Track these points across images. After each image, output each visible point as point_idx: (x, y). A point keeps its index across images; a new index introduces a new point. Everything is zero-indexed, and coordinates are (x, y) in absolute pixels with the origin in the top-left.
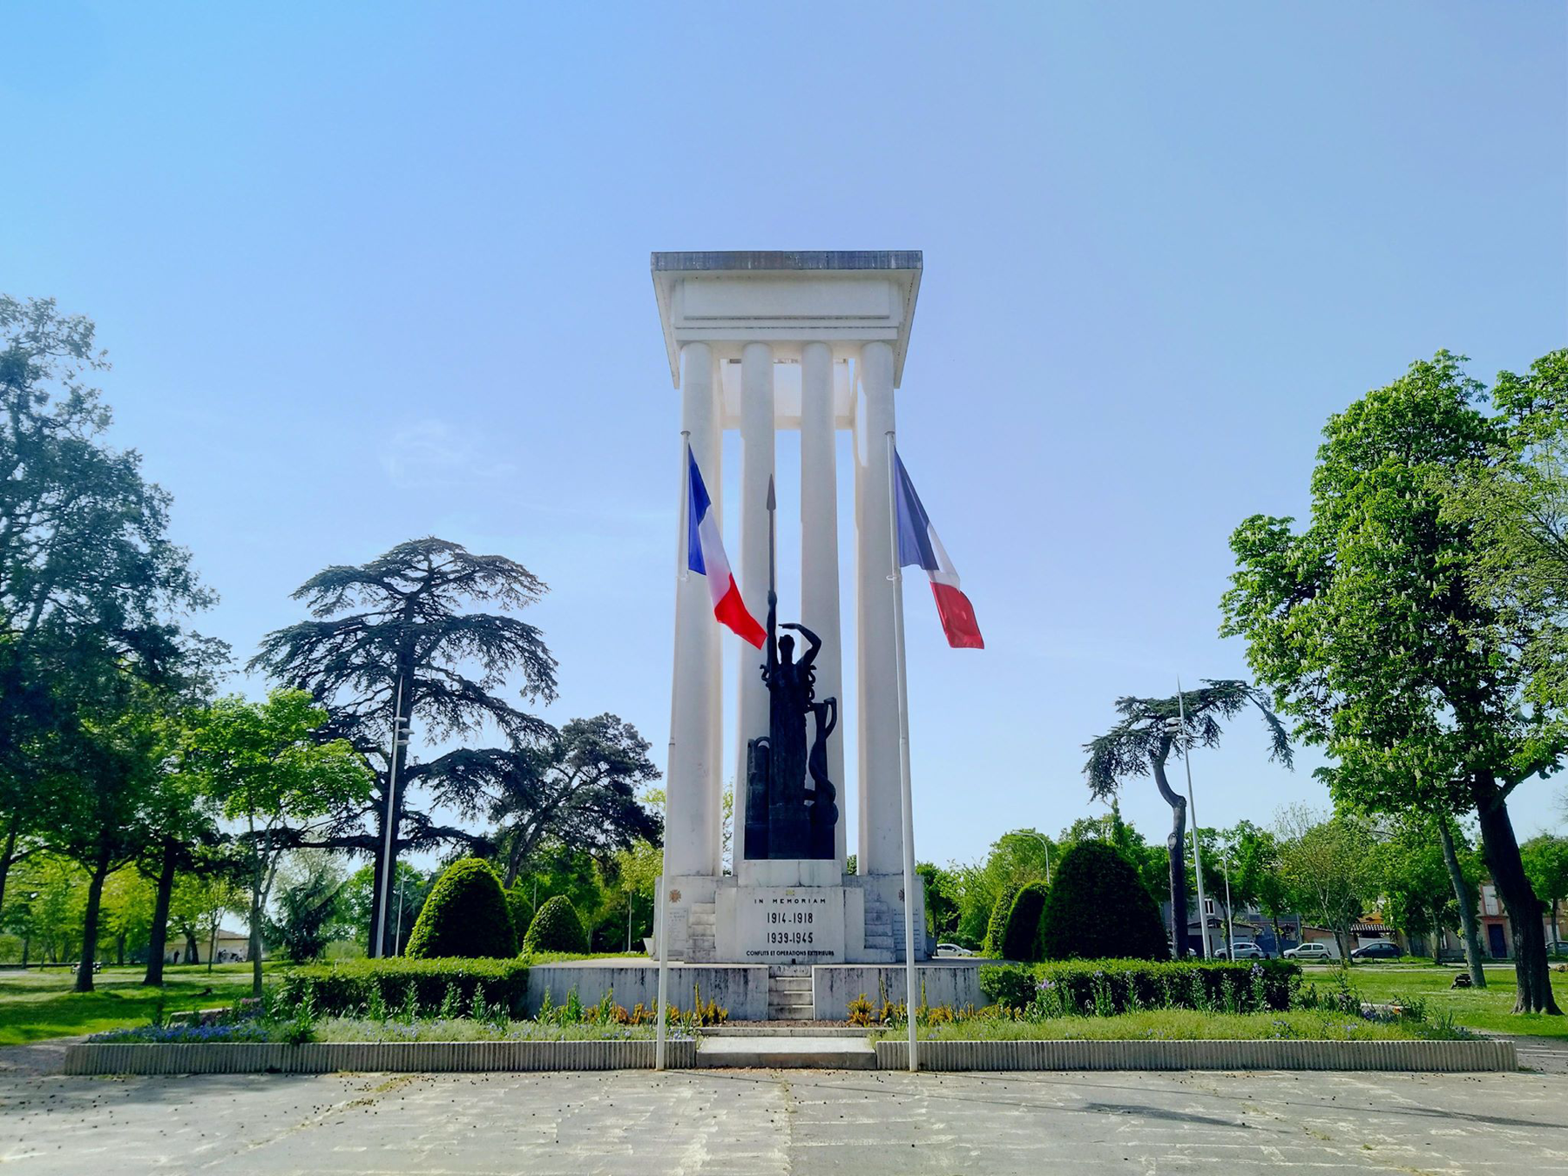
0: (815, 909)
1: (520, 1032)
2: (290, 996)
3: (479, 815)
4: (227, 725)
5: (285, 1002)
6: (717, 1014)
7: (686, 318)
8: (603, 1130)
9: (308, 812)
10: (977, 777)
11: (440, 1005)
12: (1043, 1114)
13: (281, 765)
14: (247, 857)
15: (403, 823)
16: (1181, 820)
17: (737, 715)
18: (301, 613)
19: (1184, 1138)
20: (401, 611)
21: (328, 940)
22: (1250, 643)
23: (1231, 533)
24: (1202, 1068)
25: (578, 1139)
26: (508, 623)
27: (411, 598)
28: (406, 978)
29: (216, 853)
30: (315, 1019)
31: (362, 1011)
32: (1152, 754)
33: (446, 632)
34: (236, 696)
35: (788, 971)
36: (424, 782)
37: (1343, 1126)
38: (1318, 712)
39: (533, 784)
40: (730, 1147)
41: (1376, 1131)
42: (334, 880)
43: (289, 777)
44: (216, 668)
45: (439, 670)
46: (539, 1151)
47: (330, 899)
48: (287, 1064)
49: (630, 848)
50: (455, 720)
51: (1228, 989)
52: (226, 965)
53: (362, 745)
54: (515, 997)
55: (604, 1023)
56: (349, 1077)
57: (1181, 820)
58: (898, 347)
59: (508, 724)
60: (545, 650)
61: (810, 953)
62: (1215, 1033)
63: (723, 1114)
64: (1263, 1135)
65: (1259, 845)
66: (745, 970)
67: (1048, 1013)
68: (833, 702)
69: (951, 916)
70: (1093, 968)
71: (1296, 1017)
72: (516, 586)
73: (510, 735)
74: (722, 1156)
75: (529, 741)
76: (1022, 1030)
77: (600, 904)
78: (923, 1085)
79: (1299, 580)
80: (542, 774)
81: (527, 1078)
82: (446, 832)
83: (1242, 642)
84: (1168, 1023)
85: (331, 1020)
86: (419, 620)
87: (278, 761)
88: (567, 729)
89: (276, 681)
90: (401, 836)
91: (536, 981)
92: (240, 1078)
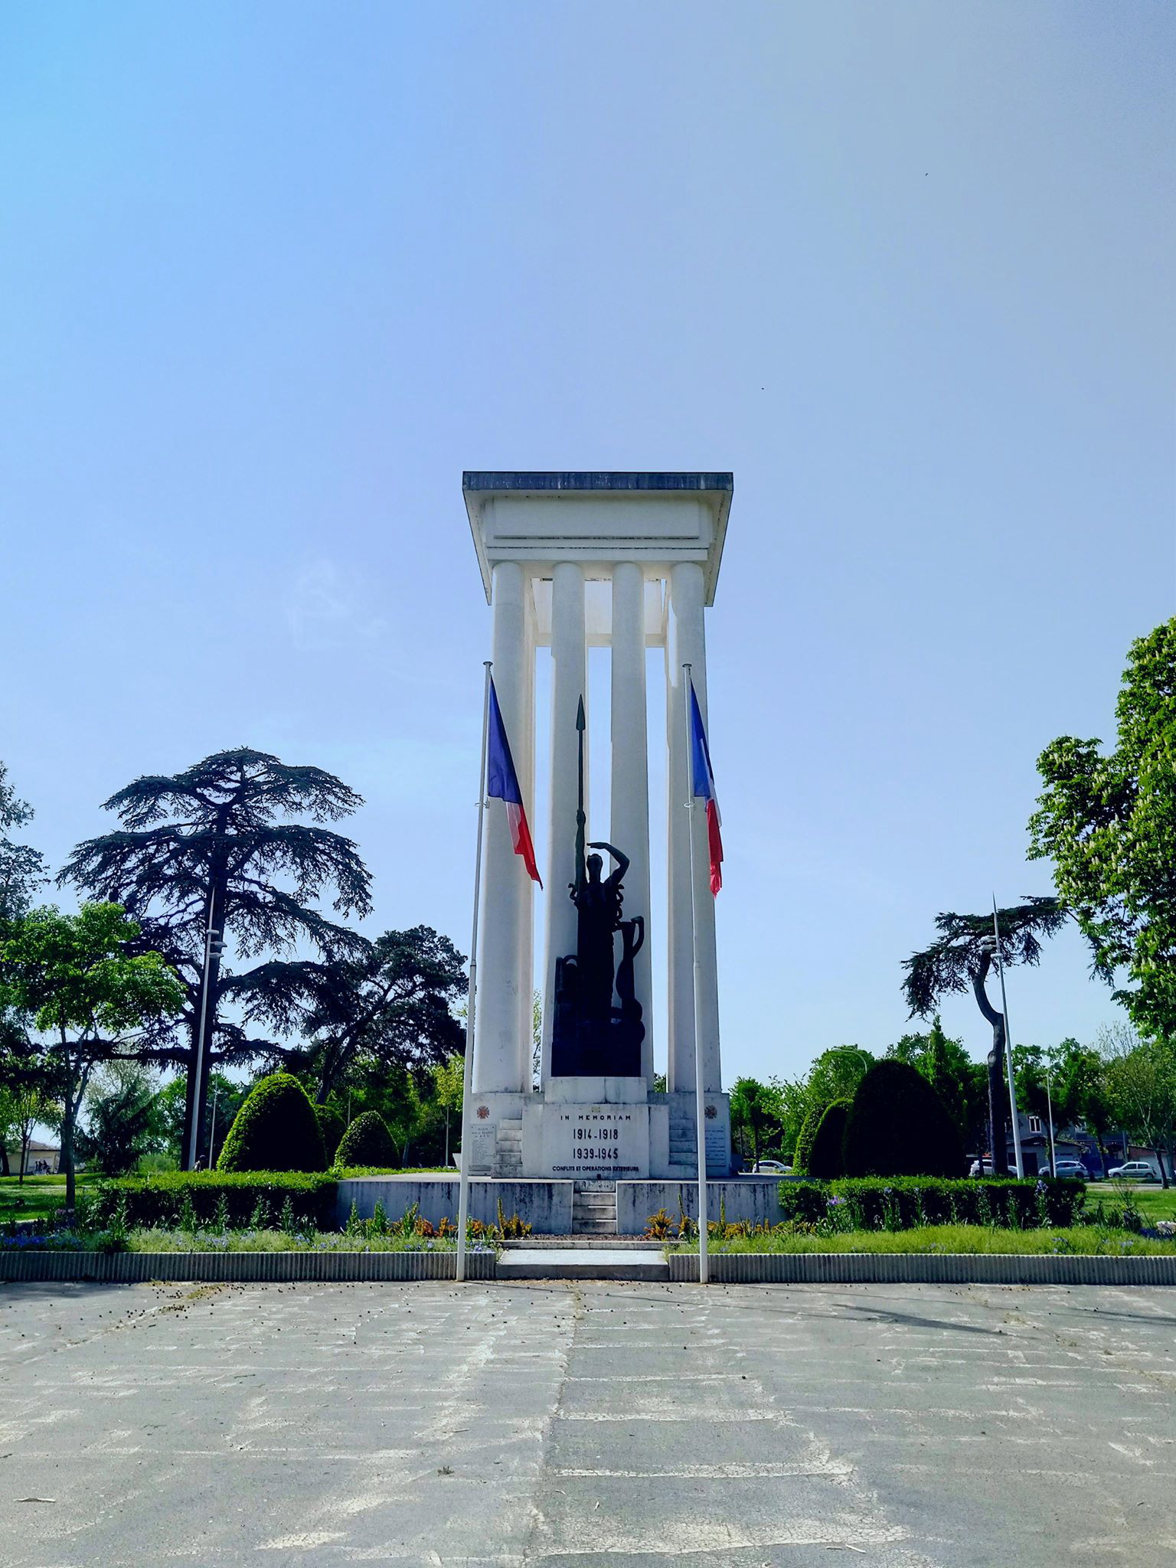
0: (621, 1126)
1: (327, 1243)
2: (104, 1206)
3: (293, 1028)
4: (39, 938)
5: (99, 1212)
6: (519, 1228)
7: (497, 538)
8: (398, 1333)
9: (119, 1024)
10: (789, 996)
11: (249, 1217)
12: (814, 1321)
13: (93, 978)
14: (59, 1067)
15: (216, 1036)
16: (1001, 1039)
17: (543, 931)
18: (112, 823)
19: (940, 1343)
20: (214, 822)
21: (142, 1152)
22: (1056, 864)
23: (1037, 755)
24: (982, 1282)
25: (373, 1341)
26: (322, 835)
27: (225, 809)
28: (216, 1191)
29: (27, 1064)
30: (129, 1229)
31: (175, 1222)
32: (971, 971)
33: (259, 845)
34: (49, 908)
35: (594, 1186)
36: (237, 995)
37: (1094, 1334)
38: (1124, 934)
39: (346, 998)
40: (515, 1348)
41: (1123, 1339)
42: (146, 1092)
43: (101, 990)
44: (27, 877)
45: (251, 881)
46: (337, 1350)
47: (143, 1111)
48: (101, 1273)
49: (445, 1063)
50: (269, 934)
51: (1016, 1208)
52: (37, 1177)
53: (173, 958)
54: (326, 1209)
55: (408, 1235)
56: (161, 1285)
57: (1001, 1039)
58: (710, 568)
59: (322, 938)
60: (359, 863)
61: (615, 1169)
62: (995, 1247)
63: (513, 1321)
64: (1015, 1341)
65: (1084, 1062)
66: (550, 1185)
67: (838, 1226)
68: (640, 921)
69: (772, 1132)
70: (884, 1184)
71: (1081, 1234)
72: (331, 798)
73: (324, 948)
74: (505, 1355)
75: (342, 953)
76: (812, 1244)
77: (416, 1119)
78: (709, 1296)
79: (1103, 802)
80: (357, 986)
81: (332, 1287)
82: (260, 1045)
83: (1049, 865)
84: (952, 1238)
85: (143, 1231)
86: (231, 831)
87: (90, 974)
88: (382, 941)
89: (87, 891)
90: (213, 1050)
91: (345, 1193)
92: (56, 1285)
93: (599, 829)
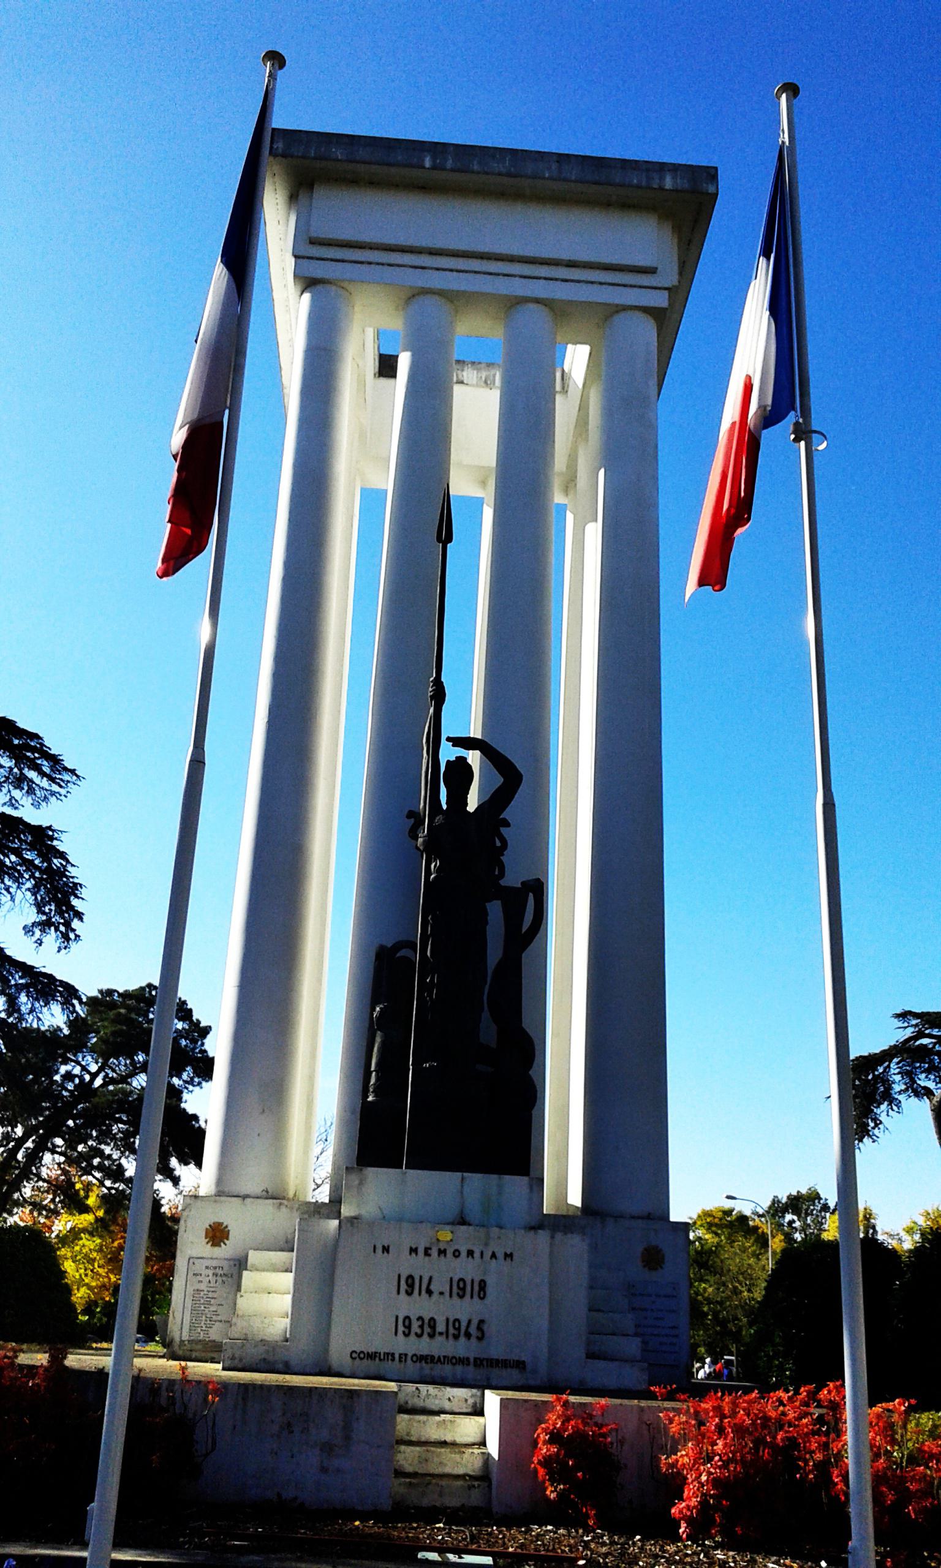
0: (495, 1274)
58: (666, 321)
61: (479, 1362)
93: (466, 713)
